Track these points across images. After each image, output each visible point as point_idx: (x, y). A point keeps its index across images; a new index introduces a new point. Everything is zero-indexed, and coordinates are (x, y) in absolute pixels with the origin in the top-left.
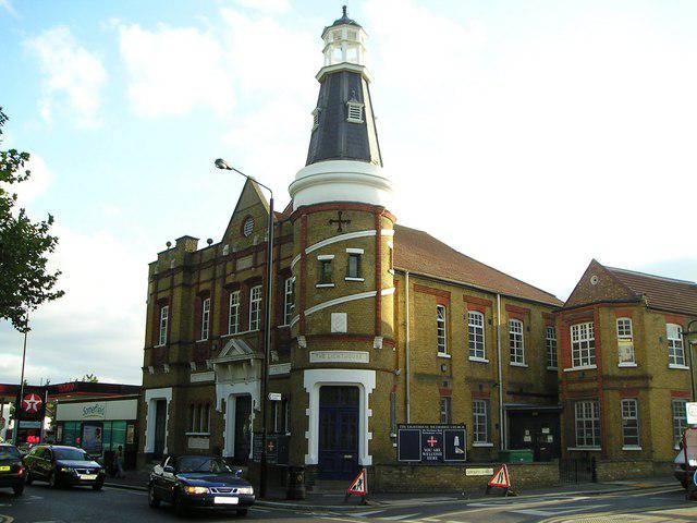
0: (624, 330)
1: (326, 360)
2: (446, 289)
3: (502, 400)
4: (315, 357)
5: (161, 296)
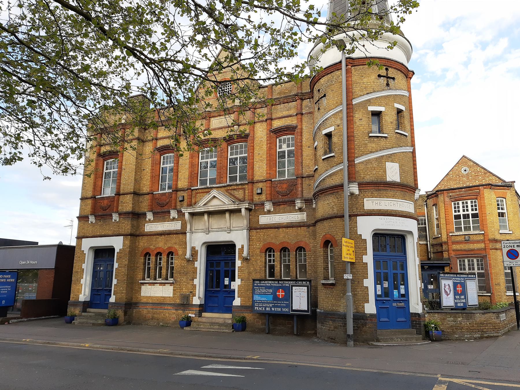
4: (370, 204)
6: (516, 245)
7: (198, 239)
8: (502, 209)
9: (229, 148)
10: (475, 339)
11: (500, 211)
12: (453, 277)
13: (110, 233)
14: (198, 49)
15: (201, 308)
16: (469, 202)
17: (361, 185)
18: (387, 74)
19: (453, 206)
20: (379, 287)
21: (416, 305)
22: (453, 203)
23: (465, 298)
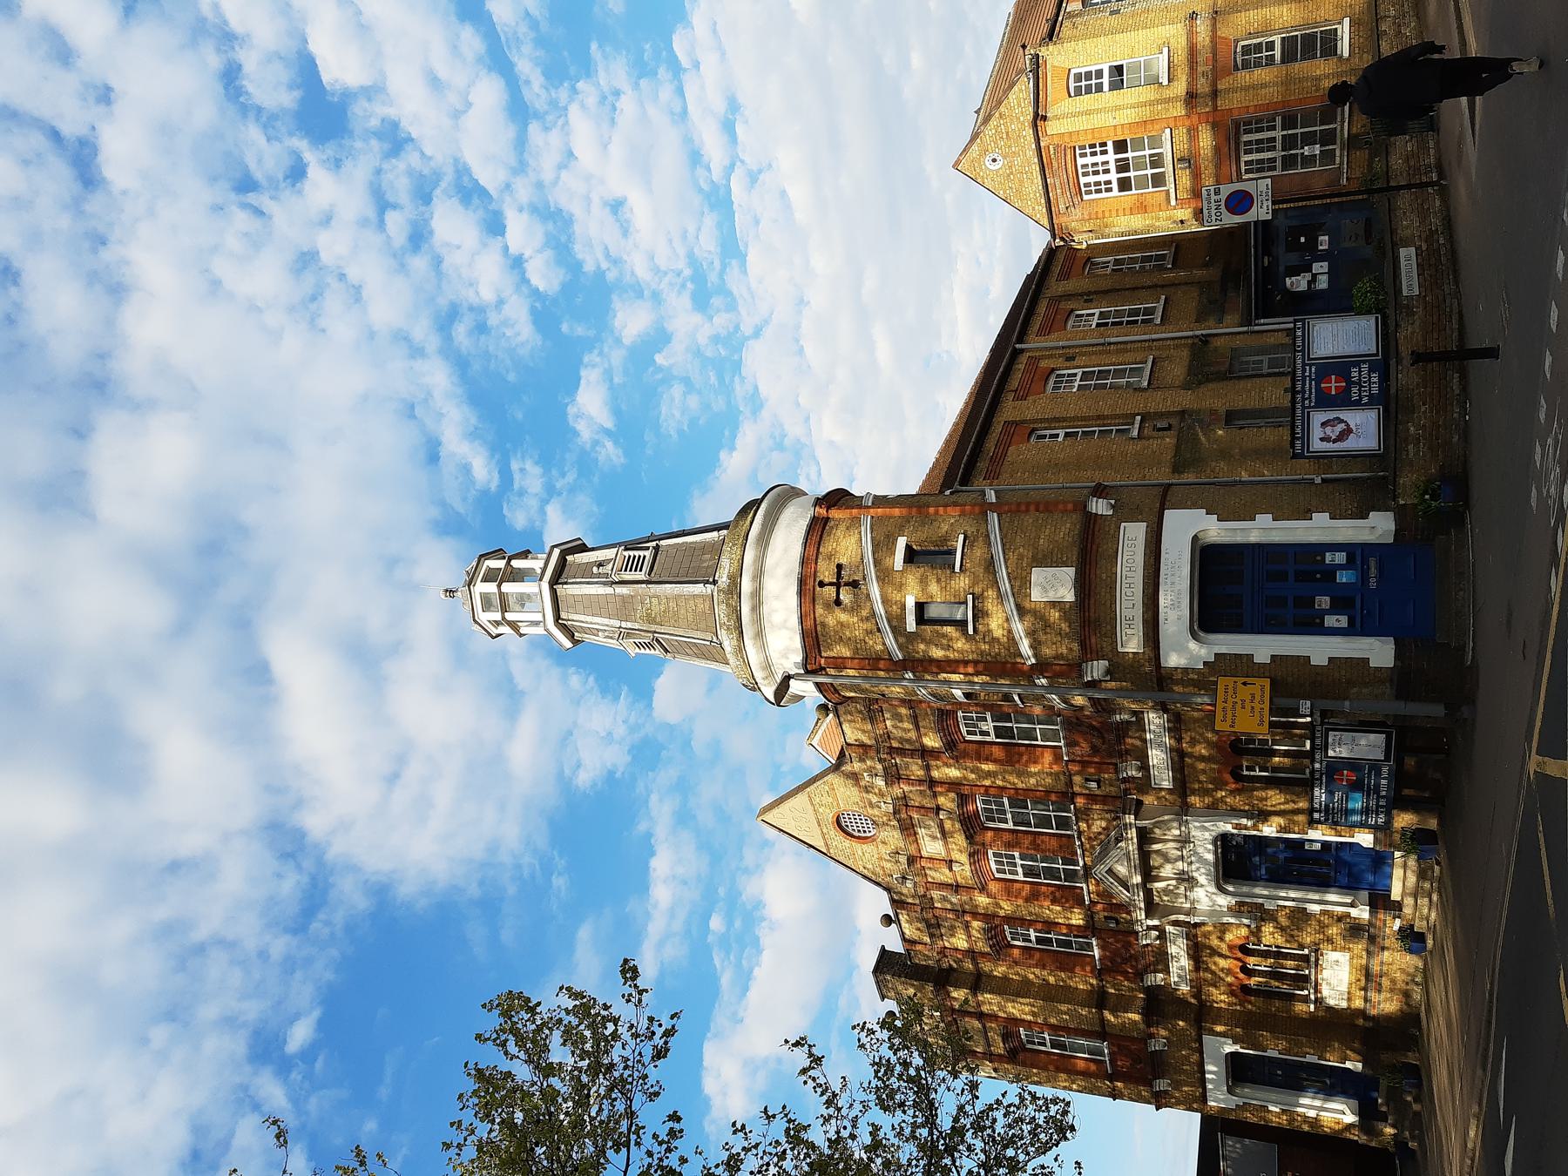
0: (1098, 149)
1: (1138, 613)
2: (997, 428)
3: (1227, 330)
4: (1132, 644)
5: (999, 1048)
6: (1213, 197)
7: (1208, 899)
8: (1099, 74)
10: (1464, 389)
11: (1106, 80)
12: (1304, 407)
15: (1380, 903)
16: (1080, 161)
17: (1088, 652)
18: (831, 584)
19: (1094, 196)
20: (1330, 621)
21: (1379, 527)
22: (1086, 197)
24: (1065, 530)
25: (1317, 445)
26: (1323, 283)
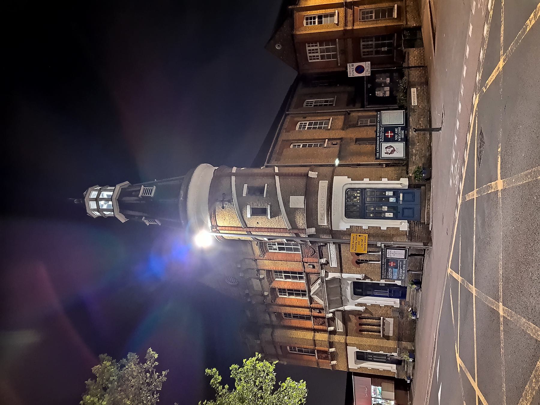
4: (323, 222)
9: (270, 251)
12: (380, 142)
13: (345, 353)
14: (94, 381)
20: (387, 215)
23: (397, 127)
24: (302, 182)
25: (384, 155)
26: (388, 94)
